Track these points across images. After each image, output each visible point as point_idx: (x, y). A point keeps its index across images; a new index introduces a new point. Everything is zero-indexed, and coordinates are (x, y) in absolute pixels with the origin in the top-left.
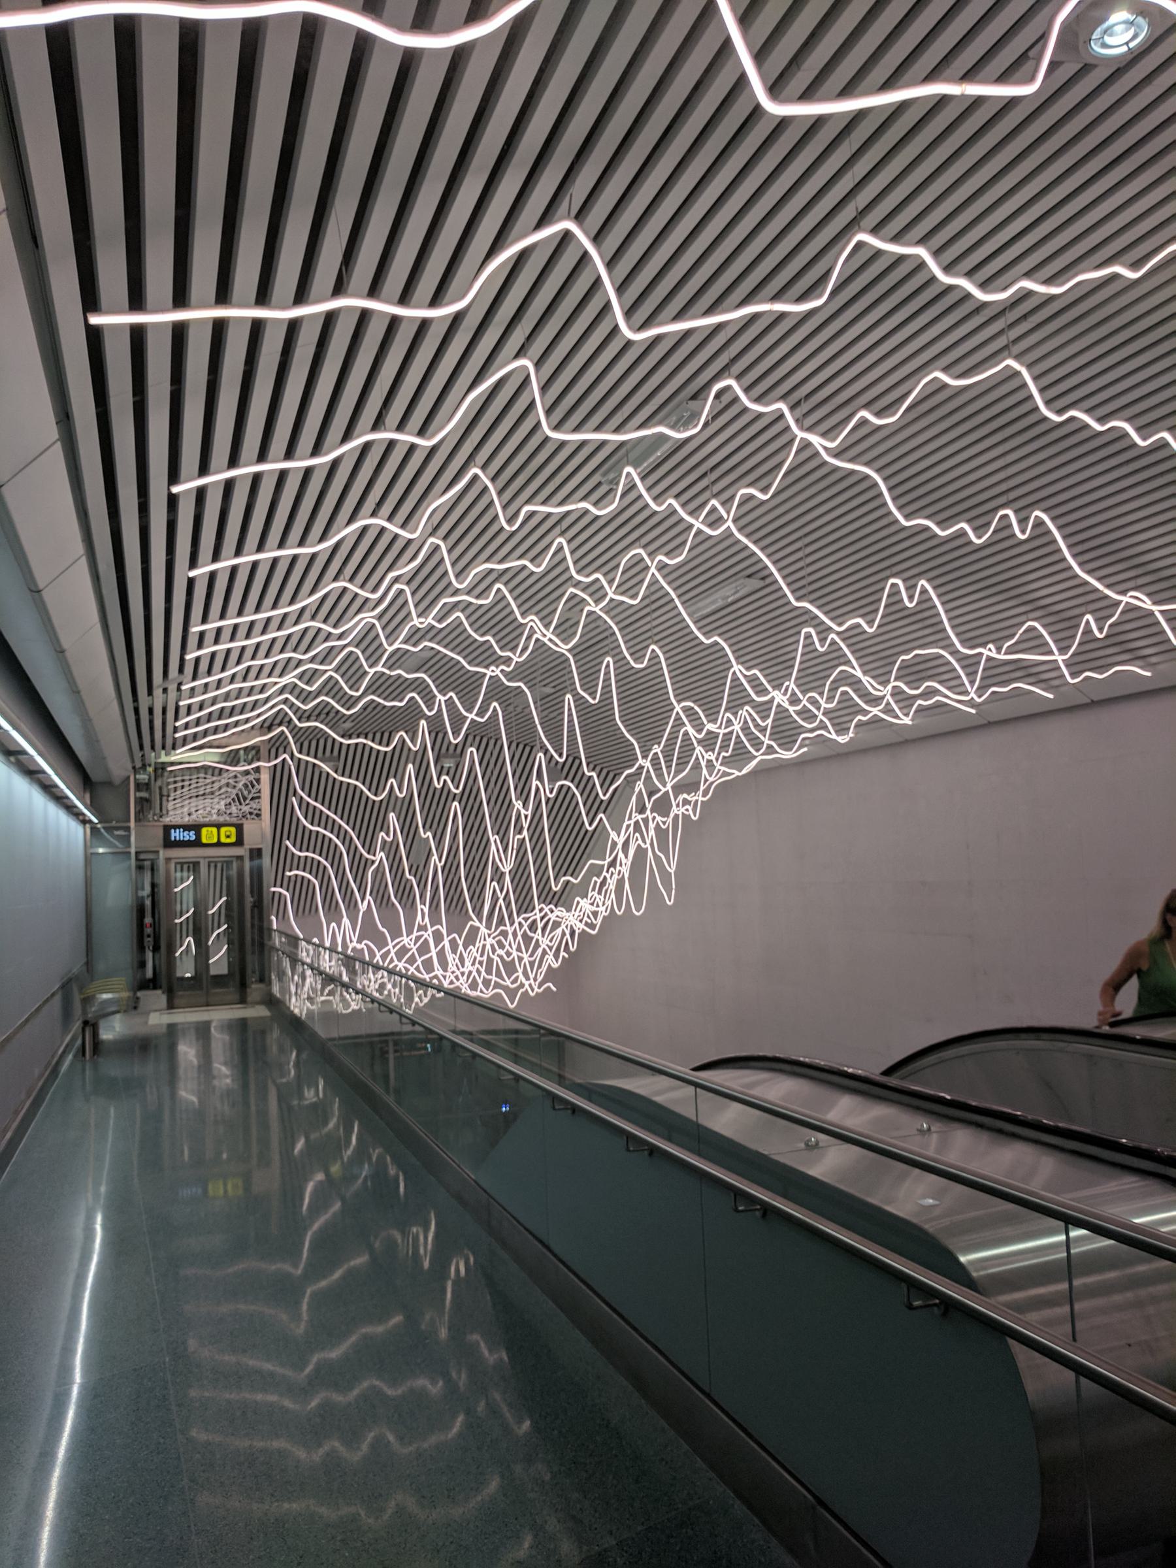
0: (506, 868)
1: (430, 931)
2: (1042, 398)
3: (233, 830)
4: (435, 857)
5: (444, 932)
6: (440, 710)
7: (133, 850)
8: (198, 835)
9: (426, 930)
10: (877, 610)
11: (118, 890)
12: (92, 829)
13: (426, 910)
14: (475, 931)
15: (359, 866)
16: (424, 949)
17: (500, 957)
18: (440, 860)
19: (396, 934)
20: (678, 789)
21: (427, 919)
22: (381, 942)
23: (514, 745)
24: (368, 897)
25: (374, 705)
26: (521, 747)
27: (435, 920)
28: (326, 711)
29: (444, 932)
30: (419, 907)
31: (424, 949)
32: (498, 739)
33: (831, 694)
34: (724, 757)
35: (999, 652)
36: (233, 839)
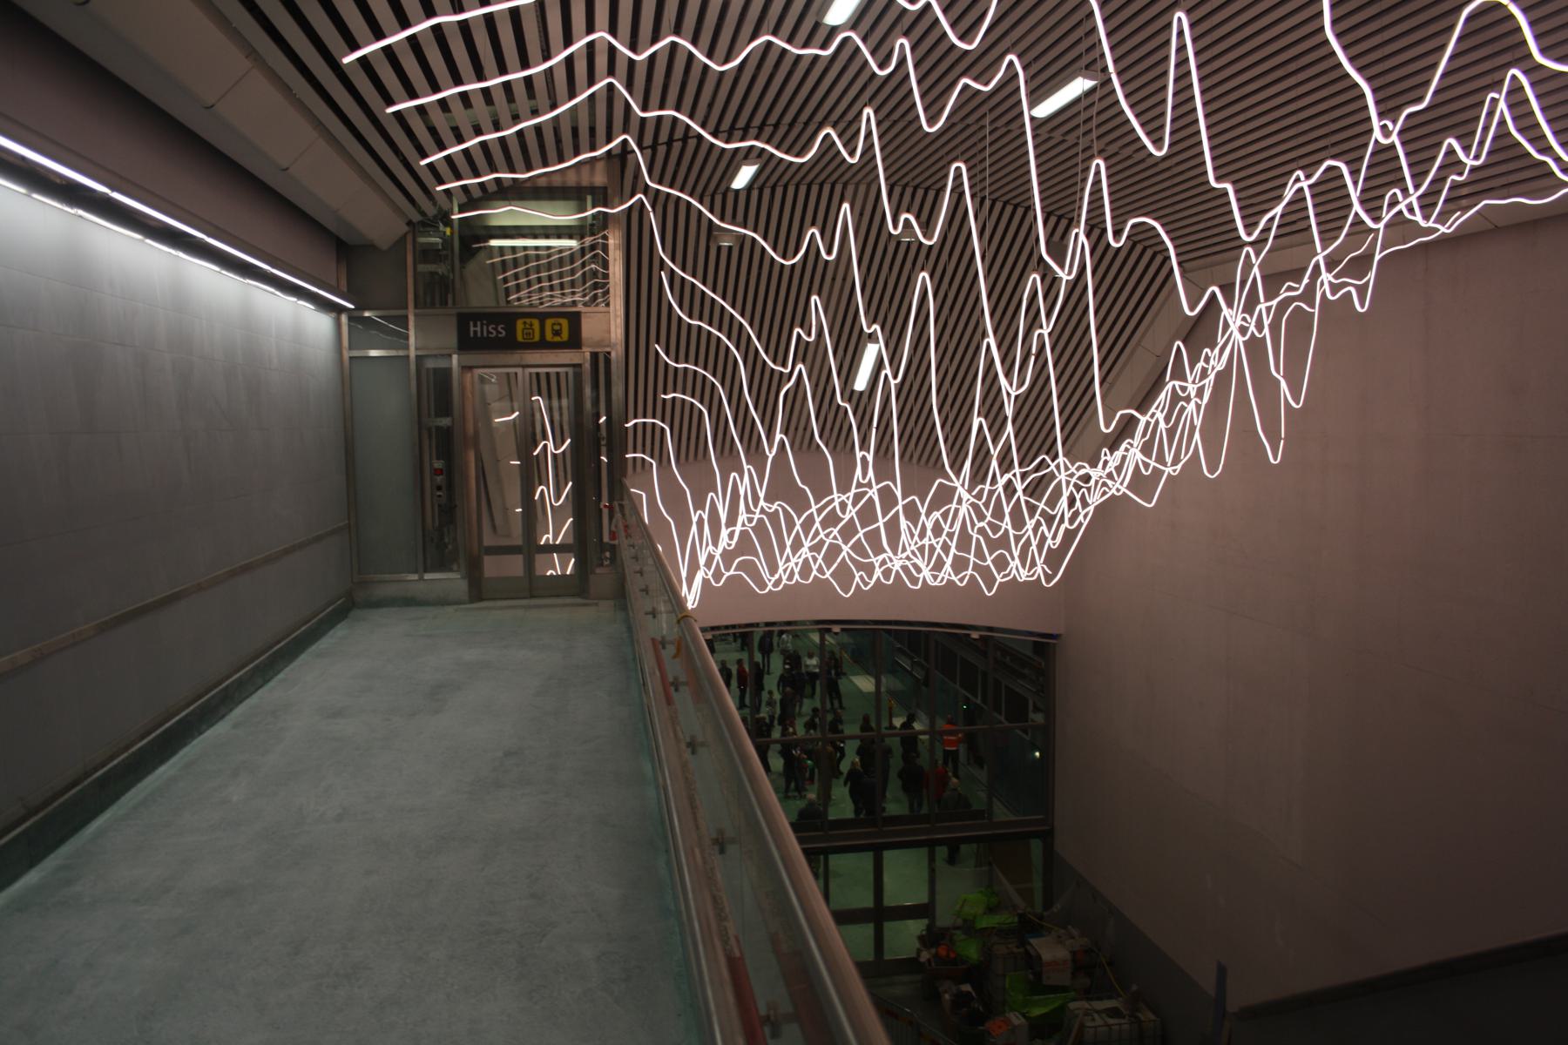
0: (1010, 390)
1: (875, 488)
2: (1533, 31)
3: (565, 322)
4: (887, 371)
5: (899, 493)
6: (869, 147)
7: (412, 353)
8: (511, 330)
9: (871, 487)
10: (1341, 228)
11: (390, 408)
12: (350, 319)
13: (870, 458)
14: (946, 495)
15: (765, 384)
16: (867, 515)
17: (982, 531)
18: (895, 377)
19: (822, 491)
20: (838, 550)
21: (871, 473)
22: (801, 505)
23: (897, 190)
24: (778, 436)
25: (797, 147)
26: (999, 205)
27: (883, 472)
28: (663, 137)
29: (899, 493)
30: (859, 454)
31: (867, 515)
32: (1030, 208)
33: (1436, 187)
34: (1455, 186)
35: (1426, 217)
36: (565, 336)
